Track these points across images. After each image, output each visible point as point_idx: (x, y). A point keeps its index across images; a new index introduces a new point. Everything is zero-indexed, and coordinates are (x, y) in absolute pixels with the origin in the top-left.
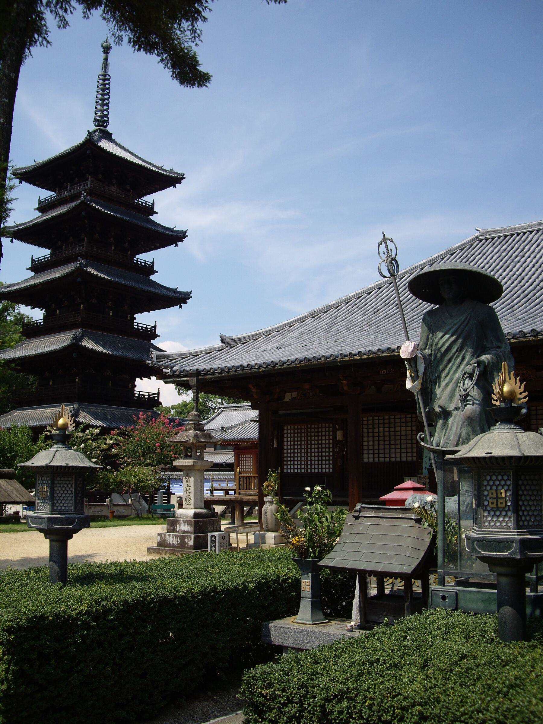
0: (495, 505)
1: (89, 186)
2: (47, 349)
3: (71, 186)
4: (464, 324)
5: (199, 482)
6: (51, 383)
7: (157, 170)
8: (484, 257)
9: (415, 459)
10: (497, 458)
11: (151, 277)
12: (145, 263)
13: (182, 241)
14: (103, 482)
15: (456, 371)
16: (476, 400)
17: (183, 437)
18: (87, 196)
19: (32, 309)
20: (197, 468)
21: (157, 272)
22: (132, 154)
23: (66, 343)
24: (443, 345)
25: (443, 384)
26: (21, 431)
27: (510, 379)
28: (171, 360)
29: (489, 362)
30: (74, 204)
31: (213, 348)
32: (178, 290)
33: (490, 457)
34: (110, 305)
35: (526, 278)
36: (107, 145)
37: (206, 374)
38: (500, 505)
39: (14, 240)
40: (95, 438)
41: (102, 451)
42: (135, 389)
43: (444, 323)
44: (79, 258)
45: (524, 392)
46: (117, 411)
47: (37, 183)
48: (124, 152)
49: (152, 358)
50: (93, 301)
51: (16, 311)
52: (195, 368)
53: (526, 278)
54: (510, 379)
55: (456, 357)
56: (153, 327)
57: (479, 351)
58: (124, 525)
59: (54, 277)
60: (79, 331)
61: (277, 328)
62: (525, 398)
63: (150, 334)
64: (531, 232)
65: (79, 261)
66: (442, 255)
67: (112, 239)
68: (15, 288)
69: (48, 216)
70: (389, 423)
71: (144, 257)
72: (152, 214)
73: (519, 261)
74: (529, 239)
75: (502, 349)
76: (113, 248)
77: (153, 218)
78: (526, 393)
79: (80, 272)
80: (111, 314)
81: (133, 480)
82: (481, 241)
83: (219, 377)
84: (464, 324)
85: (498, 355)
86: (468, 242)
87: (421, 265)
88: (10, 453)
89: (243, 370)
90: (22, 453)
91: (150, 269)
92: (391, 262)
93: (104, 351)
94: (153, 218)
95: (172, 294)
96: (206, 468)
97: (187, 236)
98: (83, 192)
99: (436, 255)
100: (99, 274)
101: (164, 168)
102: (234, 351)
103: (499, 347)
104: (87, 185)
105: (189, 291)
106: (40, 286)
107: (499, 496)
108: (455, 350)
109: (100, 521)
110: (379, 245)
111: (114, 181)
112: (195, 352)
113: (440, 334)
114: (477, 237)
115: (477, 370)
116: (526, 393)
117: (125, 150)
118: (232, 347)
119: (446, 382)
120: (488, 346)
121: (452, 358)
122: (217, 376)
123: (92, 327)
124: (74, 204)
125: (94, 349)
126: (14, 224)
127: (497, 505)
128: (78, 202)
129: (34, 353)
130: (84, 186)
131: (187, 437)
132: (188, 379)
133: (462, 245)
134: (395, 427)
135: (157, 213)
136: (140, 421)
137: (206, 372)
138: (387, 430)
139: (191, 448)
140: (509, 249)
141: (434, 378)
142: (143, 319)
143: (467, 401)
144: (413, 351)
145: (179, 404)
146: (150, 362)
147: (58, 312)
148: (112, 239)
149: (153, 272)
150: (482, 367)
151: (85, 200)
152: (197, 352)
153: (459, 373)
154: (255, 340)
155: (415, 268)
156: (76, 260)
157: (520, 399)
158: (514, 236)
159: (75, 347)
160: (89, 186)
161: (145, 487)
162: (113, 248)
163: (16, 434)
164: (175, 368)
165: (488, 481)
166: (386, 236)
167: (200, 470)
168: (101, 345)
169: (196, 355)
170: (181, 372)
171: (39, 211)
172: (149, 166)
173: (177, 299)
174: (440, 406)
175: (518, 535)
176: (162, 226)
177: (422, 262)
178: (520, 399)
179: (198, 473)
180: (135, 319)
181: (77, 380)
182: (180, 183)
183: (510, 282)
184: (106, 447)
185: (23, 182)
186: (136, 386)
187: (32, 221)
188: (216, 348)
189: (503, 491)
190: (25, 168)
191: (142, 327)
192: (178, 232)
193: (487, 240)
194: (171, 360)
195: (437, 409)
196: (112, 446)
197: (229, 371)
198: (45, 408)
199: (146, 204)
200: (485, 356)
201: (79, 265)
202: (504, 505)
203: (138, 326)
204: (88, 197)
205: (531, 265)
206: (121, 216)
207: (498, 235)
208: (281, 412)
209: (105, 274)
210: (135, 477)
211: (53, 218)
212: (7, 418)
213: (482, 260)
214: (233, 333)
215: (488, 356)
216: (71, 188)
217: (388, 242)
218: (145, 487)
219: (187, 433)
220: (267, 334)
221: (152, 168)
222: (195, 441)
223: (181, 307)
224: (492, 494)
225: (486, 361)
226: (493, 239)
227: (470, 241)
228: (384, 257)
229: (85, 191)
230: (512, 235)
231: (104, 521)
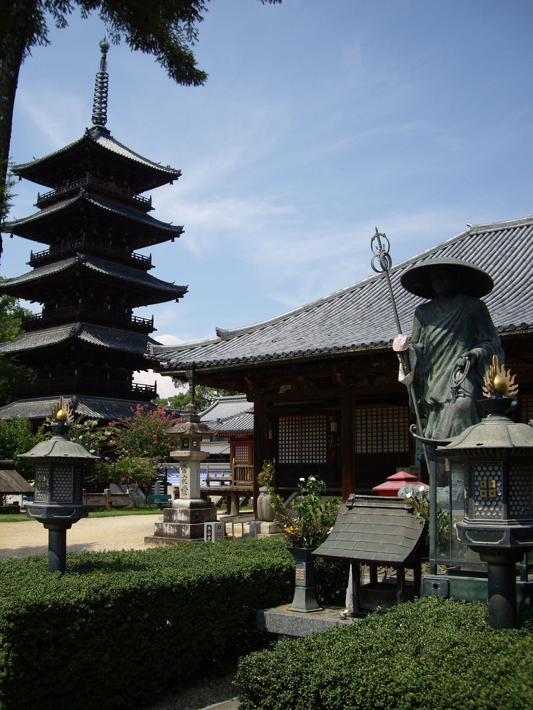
0: (486, 495)
1: (87, 182)
2: (46, 343)
3: (69, 182)
4: (456, 318)
5: (196, 473)
6: (50, 376)
7: (154, 167)
8: (475, 252)
9: (407, 450)
10: (487, 449)
11: (148, 272)
12: (142, 258)
13: (179, 236)
14: (101, 472)
15: (447, 364)
16: (467, 392)
17: (179, 428)
18: (85, 192)
19: (31, 303)
20: (193, 459)
21: (154, 267)
22: (130, 151)
23: (65, 336)
24: (435, 338)
25: (435, 376)
26: (21, 423)
27: (500, 372)
28: (168, 353)
29: (480, 355)
30: (73, 200)
31: (209, 342)
32: (174, 284)
33: (481, 449)
34: (108, 299)
35: (516, 273)
36: (105, 142)
37: (202, 367)
38: (490, 496)
39: (14, 236)
40: (93, 430)
41: (100, 442)
42: (133, 381)
43: (436, 317)
44: (78, 253)
45: (514, 384)
46: (115, 403)
47: (36, 179)
48: (122, 149)
49: (150, 351)
50: (92, 296)
51: (16, 305)
52: (191, 361)
53: (516, 273)
54: (500, 372)
55: (448, 350)
56: (150, 321)
57: (470, 344)
58: (121, 515)
59: (53, 271)
60: (77, 325)
61: (272, 321)
62: (515, 390)
63: (148, 327)
64: (521, 228)
65: (78, 256)
66: (433, 250)
67: (110, 234)
68: (15, 282)
69: (47, 212)
70: (382, 415)
71: (142, 252)
72: (149, 210)
73: (509, 256)
74: (519, 235)
75: (493, 342)
76: (111, 243)
77: (150, 213)
78: (517, 386)
79: (78, 267)
80: (109, 308)
81: (130, 471)
82: (472, 236)
83: (215, 370)
84: (456, 318)
85: (489, 348)
86: (459, 238)
87: (413, 260)
88: (10, 444)
89: (239, 362)
90: (22, 444)
91: (147, 264)
92: (384, 257)
93: (102, 344)
94: (150, 213)
95: (169, 289)
96: (202, 459)
97: (184, 232)
98: (81, 189)
99: (428, 250)
100: (97, 269)
101: (161, 165)
102: (230, 344)
103: (490, 341)
104: (86, 182)
105: (186, 285)
106: (39, 281)
107: (490, 486)
108: (447, 343)
109: (98, 511)
110: (372, 241)
111: (112, 178)
112: (192, 346)
113: (432, 328)
114: (468, 233)
115: (468, 363)
116: (517, 386)
117: (123, 147)
118: (227, 341)
119: (438, 374)
120: (479, 339)
121: (443, 351)
122: (213, 368)
123: (90, 321)
124: (73, 200)
125: (92, 342)
126: (14, 220)
127: (488, 495)
128: (77, 198)
129: (33, 346)
130: (82, 183)
131: (184, 429)
132: (185, 371)
133: (454, 240)
134: (388, 419)
135: (154, 209)
136: (138, 413)
137: (202, 365)
138: (380, 421)
139: (187, 439)
140: (499, 244)
141: (426, 371)
142: (141, 313)
143: (458, 393)
144: (405, 344)
145: (176, 396)
146: (147, 355)
147: (57, 306)
148: (110, 234)
149: (150, 267)
150: (473, 360)
151: (83, 196)
152: (194, 345)
153: (451, 366)
154: (250, 333)
155: (407, 263)
156: (74, 255)
157: (510, 391)
158: (505, 232)
159: (73, 340)
160: (87, 182)
161: (142, 478)
162: (111, 243)
163: (15, 426)
164: (172, 361)
165: (479, 472)
166: (379, 232)
167: (196, 461)
168: (99, 339)
169: (192, 348)
170: (178, 365)
171: (39, 207)
172: (146, 163)
173: (174, 293)
174: (432, 398)
175: (509, 524)
176: (159, 221)
177: (414, 257)
178: (510, 391)
179: (194, 464)
180: (132, 312)
181: (76, 373)
182: (177, 179)
183: (501, 276)
184: (104, 438)
185: (22, 179)
186: (133, 379)
187: (31, 217)
188: (212, 341)
189: (494, 482)
190: (24, 165)
191: (139, 321)
192: (175, 227)
193: (478, 235)
194: (168, 353)
195: (429, 402)
196: (109, 438)
197: (224, 364)
198: (44, 400)
199: (143, 200)
200: (476, 349)
201: (77, 260)
202: (494, 495)
203: (135, 320)
204: (87, 194)
205: (521, 260)
206: (119, 212)
207: (488, 230)
208: (275, 404)
209: (103, 269)
210: (133, 467)
211: (52, 214)
212: (7, 410)
213: (473, 255)
214: (229, 327)
215: (479, 349)
216: (69, 185)
217: (381, 237)
218: (142, 478)
219: (184, 425)
220: (262, 328)
221: (149, 165)
222: (191, 433)
223: (177, 301)
224: (483, 484)
225: (477, 354)
226: (484, 234)
227: (462, 236)
228: (377, 252)
229: (84, 187)
230: (502, 231)
231: (102, 511)
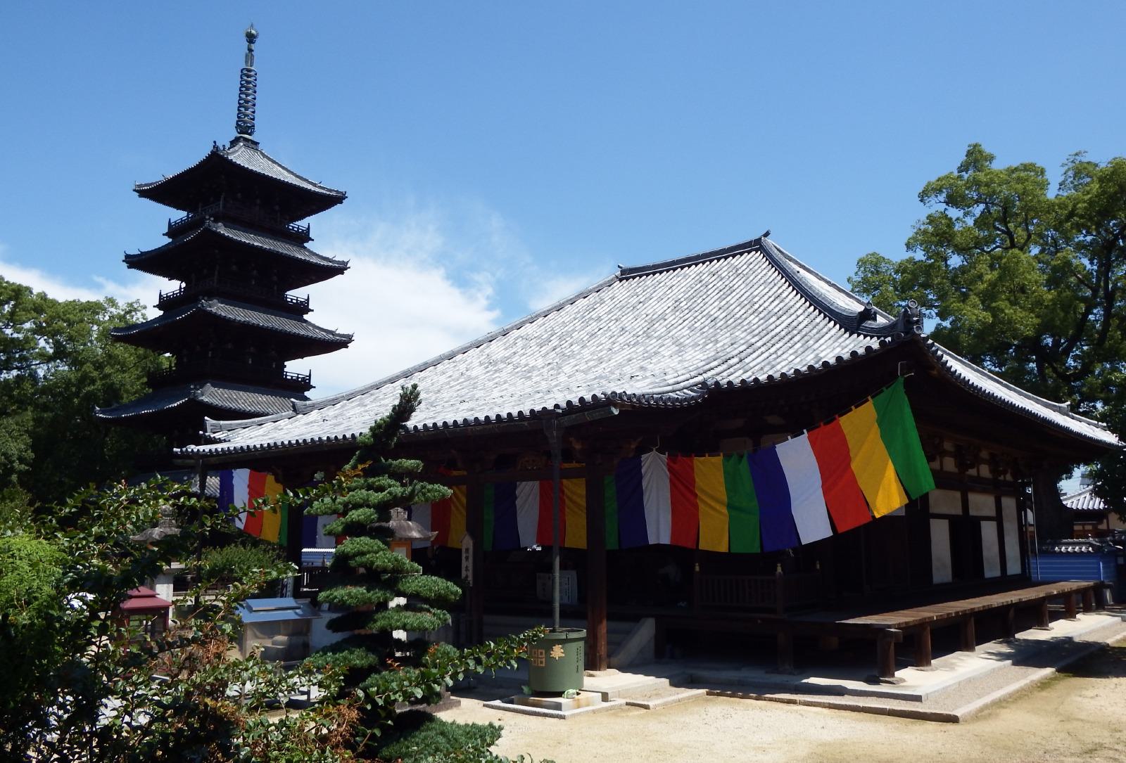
13: (343, 273)
21: (313, 311)
47: (314, 278)
117: (306, 180)
145: (467, 725)
149: (307, 310)
192: (338, 262)
